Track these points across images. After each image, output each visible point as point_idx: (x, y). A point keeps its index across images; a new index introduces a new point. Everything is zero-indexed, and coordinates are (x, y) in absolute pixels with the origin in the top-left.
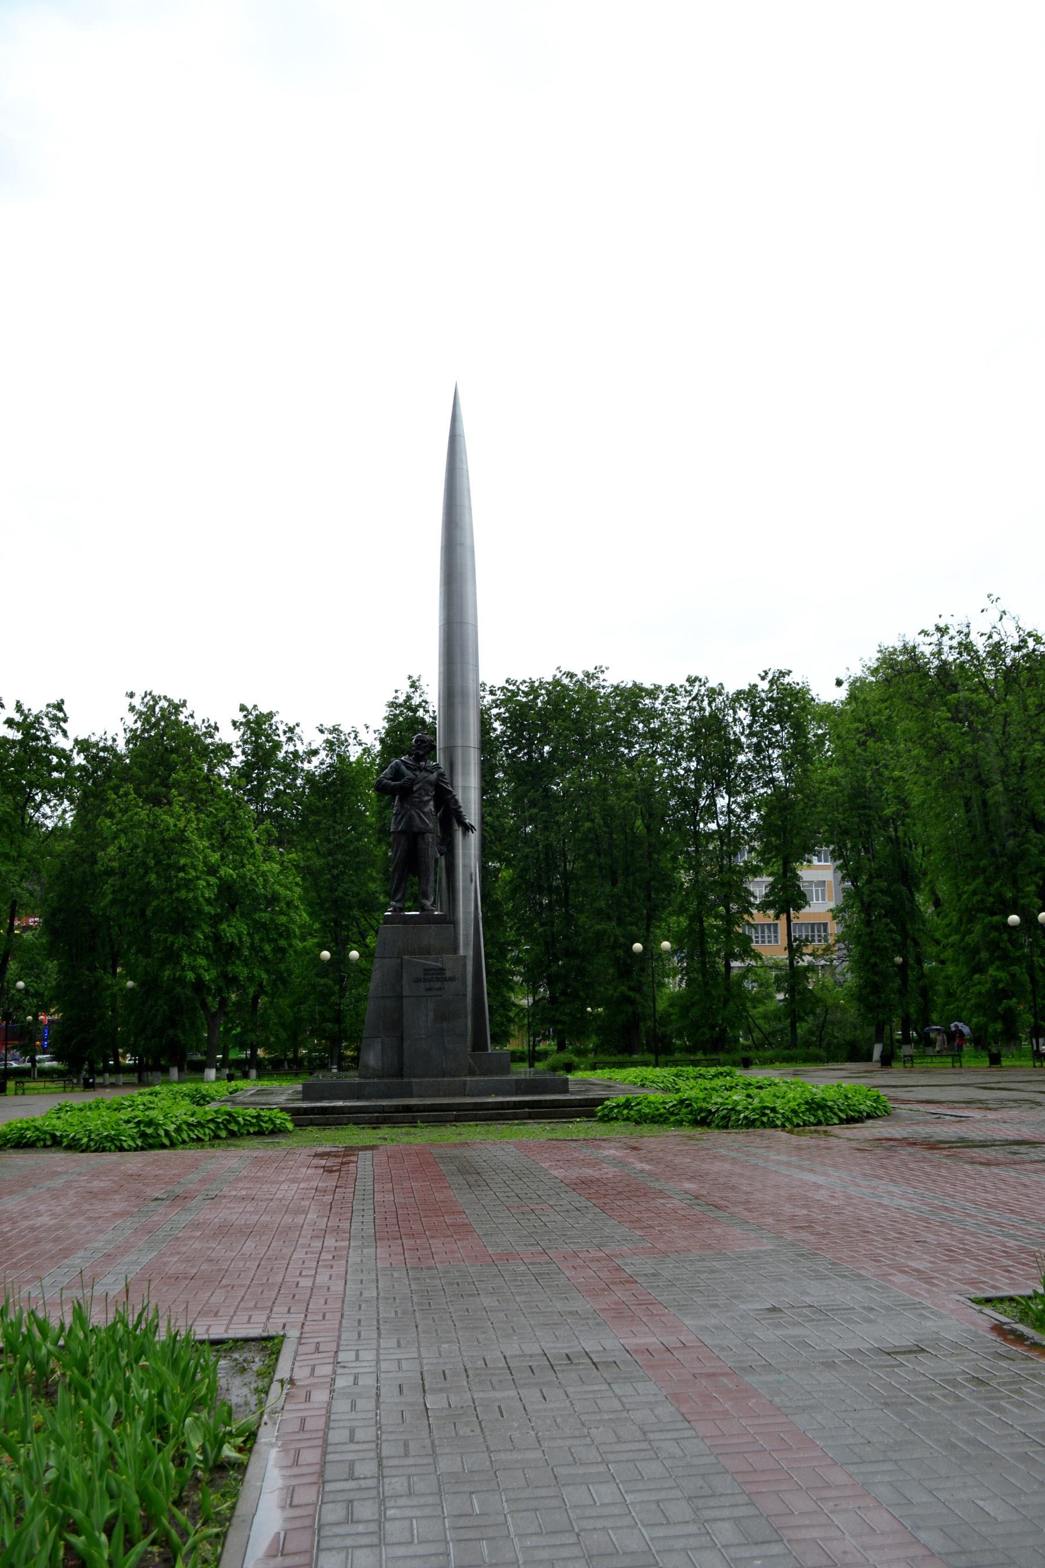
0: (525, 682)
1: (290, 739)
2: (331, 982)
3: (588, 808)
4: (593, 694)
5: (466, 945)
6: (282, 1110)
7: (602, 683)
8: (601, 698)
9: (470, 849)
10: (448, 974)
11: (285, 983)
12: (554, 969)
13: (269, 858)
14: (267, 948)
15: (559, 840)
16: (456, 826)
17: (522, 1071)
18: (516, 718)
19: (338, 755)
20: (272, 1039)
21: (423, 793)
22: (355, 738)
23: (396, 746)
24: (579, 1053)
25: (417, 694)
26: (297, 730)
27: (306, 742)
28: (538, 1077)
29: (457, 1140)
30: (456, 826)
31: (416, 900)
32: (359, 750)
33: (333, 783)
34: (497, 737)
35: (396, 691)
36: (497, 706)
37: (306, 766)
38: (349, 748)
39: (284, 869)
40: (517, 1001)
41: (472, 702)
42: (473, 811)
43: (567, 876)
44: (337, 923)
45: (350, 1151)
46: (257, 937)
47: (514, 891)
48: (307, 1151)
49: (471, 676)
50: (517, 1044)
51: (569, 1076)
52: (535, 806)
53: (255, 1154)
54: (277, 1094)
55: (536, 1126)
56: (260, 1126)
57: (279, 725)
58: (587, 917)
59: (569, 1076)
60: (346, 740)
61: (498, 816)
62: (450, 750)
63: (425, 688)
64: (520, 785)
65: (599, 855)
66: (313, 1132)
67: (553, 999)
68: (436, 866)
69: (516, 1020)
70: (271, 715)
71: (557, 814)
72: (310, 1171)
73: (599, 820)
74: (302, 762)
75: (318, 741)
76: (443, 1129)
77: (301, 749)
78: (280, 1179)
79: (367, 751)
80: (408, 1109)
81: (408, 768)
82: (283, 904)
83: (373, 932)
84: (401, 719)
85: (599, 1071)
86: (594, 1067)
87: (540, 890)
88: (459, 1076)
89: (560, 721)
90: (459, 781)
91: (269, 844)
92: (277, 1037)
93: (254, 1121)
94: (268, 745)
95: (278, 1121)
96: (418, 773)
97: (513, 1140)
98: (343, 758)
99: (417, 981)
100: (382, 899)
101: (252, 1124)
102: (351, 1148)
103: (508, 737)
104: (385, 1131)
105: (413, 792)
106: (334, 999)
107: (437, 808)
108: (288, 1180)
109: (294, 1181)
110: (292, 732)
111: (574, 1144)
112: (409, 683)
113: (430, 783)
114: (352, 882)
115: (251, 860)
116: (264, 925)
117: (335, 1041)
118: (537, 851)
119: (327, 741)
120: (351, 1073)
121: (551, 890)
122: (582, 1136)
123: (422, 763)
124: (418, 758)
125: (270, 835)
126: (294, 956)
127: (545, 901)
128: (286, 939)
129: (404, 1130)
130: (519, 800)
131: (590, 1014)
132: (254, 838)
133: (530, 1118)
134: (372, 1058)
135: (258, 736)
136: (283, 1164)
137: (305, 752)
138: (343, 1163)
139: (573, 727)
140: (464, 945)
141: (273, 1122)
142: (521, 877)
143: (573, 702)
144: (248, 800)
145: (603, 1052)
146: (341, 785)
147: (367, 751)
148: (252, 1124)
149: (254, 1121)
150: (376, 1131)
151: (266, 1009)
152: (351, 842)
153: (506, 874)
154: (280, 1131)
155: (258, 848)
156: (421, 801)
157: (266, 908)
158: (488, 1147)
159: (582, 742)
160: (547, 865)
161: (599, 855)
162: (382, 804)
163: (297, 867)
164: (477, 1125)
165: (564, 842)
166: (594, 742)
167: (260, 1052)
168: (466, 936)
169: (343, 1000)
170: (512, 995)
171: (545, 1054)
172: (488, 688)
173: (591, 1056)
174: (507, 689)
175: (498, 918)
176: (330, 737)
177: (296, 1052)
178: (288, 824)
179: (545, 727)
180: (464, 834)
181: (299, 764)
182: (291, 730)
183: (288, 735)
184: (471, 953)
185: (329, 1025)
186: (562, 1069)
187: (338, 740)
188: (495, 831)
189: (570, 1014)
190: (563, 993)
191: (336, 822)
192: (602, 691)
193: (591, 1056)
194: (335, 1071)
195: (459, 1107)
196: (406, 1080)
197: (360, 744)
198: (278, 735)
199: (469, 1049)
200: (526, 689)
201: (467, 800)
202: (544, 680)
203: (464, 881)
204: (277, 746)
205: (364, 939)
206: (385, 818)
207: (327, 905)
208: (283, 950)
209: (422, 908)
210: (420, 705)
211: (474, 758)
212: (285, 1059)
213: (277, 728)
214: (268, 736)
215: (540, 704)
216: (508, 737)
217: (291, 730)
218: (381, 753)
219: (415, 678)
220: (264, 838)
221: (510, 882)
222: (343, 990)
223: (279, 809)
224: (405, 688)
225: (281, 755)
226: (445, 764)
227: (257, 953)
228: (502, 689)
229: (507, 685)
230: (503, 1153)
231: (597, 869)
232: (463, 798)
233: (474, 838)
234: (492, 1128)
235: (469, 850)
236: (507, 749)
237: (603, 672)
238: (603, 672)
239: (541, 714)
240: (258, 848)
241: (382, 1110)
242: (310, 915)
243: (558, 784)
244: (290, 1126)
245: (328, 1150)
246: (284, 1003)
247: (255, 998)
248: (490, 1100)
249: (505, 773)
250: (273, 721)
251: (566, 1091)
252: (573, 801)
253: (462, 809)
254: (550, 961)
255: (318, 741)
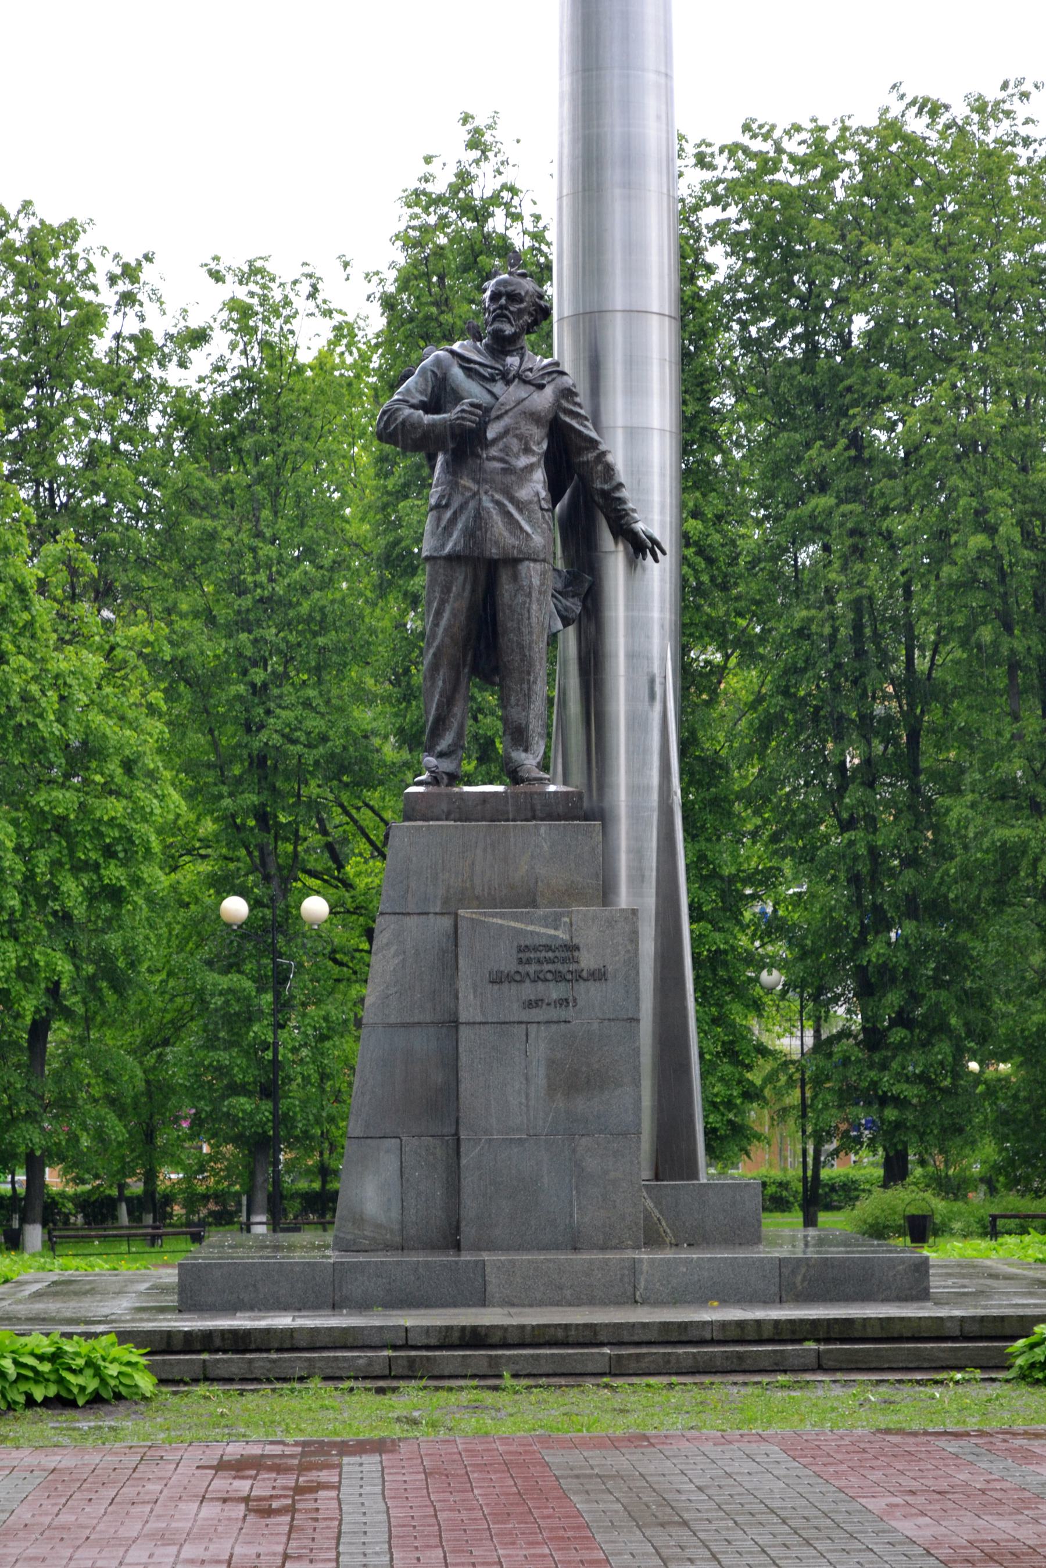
0: (798, 129)
1: (127, 299)
2: (248, 984)
3: (977, 492)
4: (994, 164)
5: (637, 878)
6: (124, 1337)
7: (1024, 131)
8: (1020, 172)
9: (647, 608)
10: (587, 961)
11: (119, 985)
12: (875, 952)
13: (72, 636)
14: (72, 888)
15: (892, 587)
16: (607, 539)
17: (786, 1236)
18: (773, 233)
19: (265, 345)
20: (85, 1142)
21: (515, 445)
22: (312, 295)
23: (428, 318)
24: (952, 1188)
25: (487, 168)
26: (147, 273)
27: (172, 307)
28: (835, 1252)
29: (619, 1427)
30: (607, 539)
31: (485, 752)
32: (325, 328)
33: (251, 426)
34: (716, 293)
35: (428, 160)
36: (716, 200)
37: (174, 376)
38: (295, 324)
39: (115, 669)
40: (766, 1040)
41: (653, 180)
42: (656, 498)
43: (915, 688)
44: (263, 818)
45: (319, 1453)
46: (42, 858)
47: (766, 728)
48: (195, 1455)
49: (651, 105)
50: (773, 1158)
51: (926, 1252)
52: (823, 487)
53: (52, 1461)
54: (104, 1293)
55: (837, 1391)
56: (61, 1381)
57: (96, 260)
58: (973, 805)
59: (926, 1252)
60: (287, 302)
61: (719, 518)
62: (591, 323)
63: (509, 150)
64: (783, 427)
65: (1008, 628)
66: (209, 1400)
67: (873, 1038)
68: (552, 661)
69: (767, 1092)
70: (70, 231)
71: (886, 511)
72: (210, 1510)
73: (1009, 530)
74: (162, 365)
75: (206, 304)
76: (573, 1394)
77: (159, 327)
78: (123, 1532)
79: (344, 332)
80: (474, 1338)
81: (469, 372)
82: (114, 767)
83: (363, 846)
84: (442, 240)
85: (1010, 1240)
86: (991, 1229)
87: (839, 729)
88: (619, 1247)
89: (898, 244)
90: (617, 410)
91: (74, 598)
92: (100, 1136)
93: (45, 1367)
94: (66, 317)
95: (113, 1370)
96: (498, 388)
97: (775, 1429)
98: (275, 355)
99: (498, 979)
100: (390, 751)
101: (39, 1377)
102: (322, 1447)
103: (748, 289)
104: (411, 1399)
105: (487, 444)
106: (259, 1030)
107: (555, 491)
108: (151, 1536)
109: (163, 1538)
110: (134, 280)
111: (953, 1446)
112: (463, 135)
113: (534, 417)
114: (307, 704)
115: (24, 642)
116: (60, 825)
117: (260, 1146)
118: (832, 617)
119: (233, 304)
120: (307, 1236)
121: (867, 726)
122: (972, 1423)
123: (513, 361)
124: (502, 345)
125: (74, 572)
126: (145, 912)
127: (853, 761)
128: (124, 864)
129: (465, 1397)
130: (777, 471)
131: (977, 1078)
132: (31, 582)
133: (820, 1368)
134: (371, 1190)
135: (34, 288)
136: (129, 1491)
137: (170, 337)
138: (299, 1490)
139: (937, 260)
140: (631, 879)
141: (98, 1372)
142: (786, 692)
143: (936, 188)
144: (13, 474)
145: (1013, 1183)
146: (273, 430)
147: (344, 332)
148: (39, 1377)
149: (45, 1367)
150: (387, 1399)
151: (68, 1060)
152: (305, 592)
153: (740, 683)
154: (118, 1397)
155: (43, 608)
156: (509, 470)
157: (67, 776)
158: (708, 1447)
159: (964, 300)
160: (860, 654)
161: (1008, 628)
162: (390, 483)
163: (151, 661)
164: (671, 1386)
165: (908, 595)
166: (996, 302)
167: (53, 1179)
168: (637, 853)
169: (283, 1035)
170: (754, 1023)
171: (847, 1193)
172: (690, 150)
173: (977, 1197)
174: (746, 150)
175: (719, 805)
176: (241, 293)
177: (150, 1177)
178: (128, 541)
179: (854, 261)
180: (632, 564)
181: (155, 372)
182: (130, 272)
183: (123, 286)
184: (649, 902)
185: (244, 1103)
186: (900, 1232)
187: (264, 300)
188: (710, 561)
189: (923, 1078)
190: (902, 1019)
191: (259, 535)
192: (1023, 154)
193: (977, 1197)
194: (260, 1230)
195: (618, 1336)
196: (466, 1257)
197: (328, 313)
198: (94, 288)
199: (646, 1173)
200: (801, 151)
201: (639, 467)
202: (853, 124)
203: (631, 698)
204: (91, 319)
205: (340, 867)
206: (398, 524)
207: (237, 770)
208: (115, 895)
209: (514, 775)
210: (495, 199)
211: (659, 341)
212: (121, 1197)
213: (90, 268)
214: (64, 291)
215: (840, 194)
216: (748, 289)
217: (130, 272)
218: (386, 341)
219: (480, 122)
220: (59, 579)
221: (753, 706)
222: (282, 1005)
223: (100, 499)
224: (454, 153)
225: (101, 346)
226: (576, 361)
227: (42, 901)
228: (732, 150)
229: (745, 140)
230: (748, 1466)
231: (1000, 671)
232: (630, 462)
233: (659, 576)
234: (675, 1397)
235: (643, 605)
236: (744, 325)
237: (1025, 96)
238: (1025, 96)
239: (841, 223)
240: (43, 608)
241: (404, 1341)
242: (190, 796)
243: (891, 427)
244: (145, 1382)
245: (256, 1450)
246: (112, 1040)
247: (39, 1030)
248: (706, 1316)
249: (741, 395)
250: (78, 248)
251: (922, 1295)
252: (933, 475)
253: (624, 493)
254: (864, 930)
255: (206, 304)
